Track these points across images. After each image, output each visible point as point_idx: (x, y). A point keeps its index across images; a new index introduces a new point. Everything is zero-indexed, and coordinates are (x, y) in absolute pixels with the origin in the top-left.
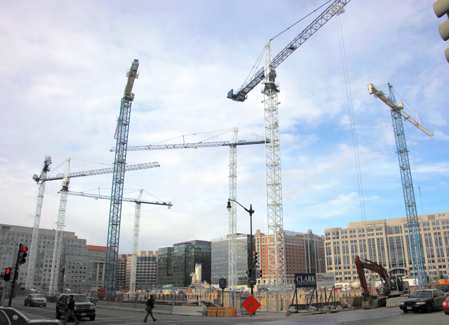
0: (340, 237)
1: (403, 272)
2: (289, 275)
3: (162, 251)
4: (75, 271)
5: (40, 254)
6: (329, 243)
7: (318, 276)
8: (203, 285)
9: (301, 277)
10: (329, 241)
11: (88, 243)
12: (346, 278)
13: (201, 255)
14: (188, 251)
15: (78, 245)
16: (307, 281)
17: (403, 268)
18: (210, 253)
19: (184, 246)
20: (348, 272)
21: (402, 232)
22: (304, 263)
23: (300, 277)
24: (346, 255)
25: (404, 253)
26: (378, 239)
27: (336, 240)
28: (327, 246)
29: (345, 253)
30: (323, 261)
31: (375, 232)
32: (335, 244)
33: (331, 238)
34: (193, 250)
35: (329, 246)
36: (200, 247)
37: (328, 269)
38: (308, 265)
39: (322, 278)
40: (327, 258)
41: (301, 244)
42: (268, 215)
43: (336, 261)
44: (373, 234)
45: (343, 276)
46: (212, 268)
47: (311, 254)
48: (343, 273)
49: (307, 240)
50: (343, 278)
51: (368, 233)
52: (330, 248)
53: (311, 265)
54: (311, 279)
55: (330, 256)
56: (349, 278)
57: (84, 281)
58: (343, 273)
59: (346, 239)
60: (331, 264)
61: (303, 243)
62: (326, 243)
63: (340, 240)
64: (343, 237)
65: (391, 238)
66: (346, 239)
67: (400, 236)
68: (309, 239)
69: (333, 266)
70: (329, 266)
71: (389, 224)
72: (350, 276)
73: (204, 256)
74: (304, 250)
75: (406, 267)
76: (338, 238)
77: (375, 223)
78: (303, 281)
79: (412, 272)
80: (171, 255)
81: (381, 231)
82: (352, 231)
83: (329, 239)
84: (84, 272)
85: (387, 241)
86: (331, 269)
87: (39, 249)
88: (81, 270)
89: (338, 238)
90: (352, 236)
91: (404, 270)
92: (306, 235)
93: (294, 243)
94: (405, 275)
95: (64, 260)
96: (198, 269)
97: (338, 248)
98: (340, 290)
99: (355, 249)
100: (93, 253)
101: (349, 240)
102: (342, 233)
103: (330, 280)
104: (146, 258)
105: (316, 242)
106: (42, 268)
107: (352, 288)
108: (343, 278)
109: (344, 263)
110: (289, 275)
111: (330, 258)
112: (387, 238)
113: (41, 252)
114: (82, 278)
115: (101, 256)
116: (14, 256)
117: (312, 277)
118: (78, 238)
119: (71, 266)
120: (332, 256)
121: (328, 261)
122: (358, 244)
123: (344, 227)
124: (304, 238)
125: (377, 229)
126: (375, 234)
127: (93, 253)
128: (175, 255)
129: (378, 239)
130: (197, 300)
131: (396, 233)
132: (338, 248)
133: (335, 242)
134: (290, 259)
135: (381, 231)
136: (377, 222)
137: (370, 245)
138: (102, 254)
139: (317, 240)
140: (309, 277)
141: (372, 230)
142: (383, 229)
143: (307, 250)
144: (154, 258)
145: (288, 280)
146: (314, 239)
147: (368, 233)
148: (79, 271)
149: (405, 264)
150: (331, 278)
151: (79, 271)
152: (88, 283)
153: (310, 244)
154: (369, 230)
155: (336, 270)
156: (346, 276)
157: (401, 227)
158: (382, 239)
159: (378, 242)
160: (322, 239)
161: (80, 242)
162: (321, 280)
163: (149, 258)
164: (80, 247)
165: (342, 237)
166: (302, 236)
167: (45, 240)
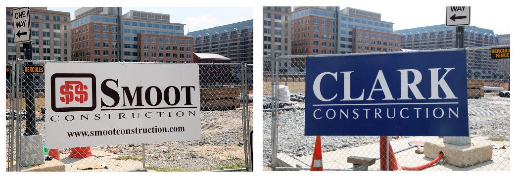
7: (60, 82)
9: (347, 75)
11: (172, 21)
16: (388, 96)
23: (341, 77)
39: (100, 94)
54: (425, 86)
78: (354, 94)
103: (163, 103)
117: (434, 72)
118: (171, 21)
130: (26, 33)
140: (404, 73)
150: (172, 93)
162: (89, 103)
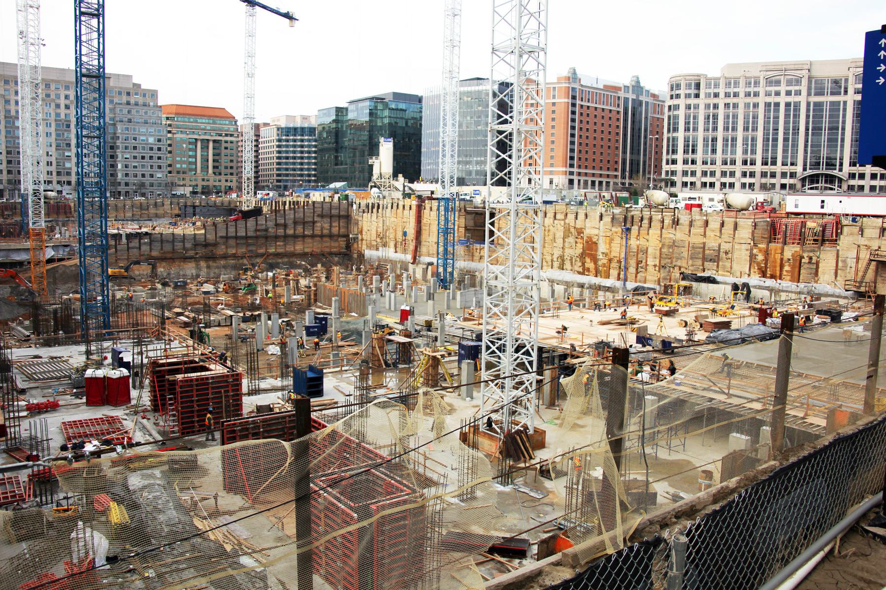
0: (702, 95)
1: (832, 182)
2: (583, 171)
3: (325, 114)
4: (139, 156)
5: (60, 120)
6: (677, 107)
8: (396, 184)
10: (675, 102)
11: (143, 87)
12: (704, 185)
13: (402, 124)
14: (376, 114)
15: (141, 102)
17: (836, 172)
18: (421, 118)
19: (367, 103)
20: (711, 172)
21: (846, 92)
22: (617, 148)
24: (710, 134)
25: (843, 140)
26: (788, 105)
27: (692, 101)
28: (671, 113)
29: (708, 130)
30: (659, 147)
31: (783, 88)
32: (690, 108)
33: (683, 96)
34: (386, 113)
35: (676, 113)
36: (402, 106)
37: (667, 163)
38: (624, 152)
40: (668, 139)
41: (614, 106)
42: (494, 11)
43: (686, 146)
44: (778, 94)
45: (698, 179)
46: (423, 150)
47: (633, 129)
48: (699, 174)
49: (628, 99)
50: (698, 184)
51: (769, 89)
52: (676, 117)
53: (632, 153)
55: (675, 135)
56: (711, 183)
57: (159, 175)
58: (699, 174)
59: (716, 101)
60: (674, 152)
61: (618, 106)
62: (670, 107)
63: (702, 101)
64: (710, 94)
65: (818, 105)
66: (716, 101)
67: (839, 102)
68: (631, 96)
69: (680, 156)
70: (669, 157)
71: (817, 73)
72: (712, 180)
73: (409, 124)
74: (618, 120)
75: (841, 170)
76: (697, 96)
77: (788, 67)
79: (852, 182)
80: (342, 122)
81: (797, 88)
82: (730, 83)
83: (678, 96)
84: (159, 158)
85: (808, 110)
86: (674, 162)
87: (58, 111)
88: (151, 153)
89: (697, 96)
90: (729, 93)
91: (835, 177)
92: (626, 87)
93: (592, 102)
94: (836, 187)
95: (115, 133)
96: (386, 148)
97: (695, 118)
98: (698, 209)
99: (733, 123)
100: (186, 120)
101: (721, 101)
102: (708, 85)
104: (295, 129)
105: (647, 103)
106: (70, 150)
107: (729, 206)
108: (698, 184)
109: (705, 152)
110: (583, 171)
111: (675, 139)
112: (808, 104)
113: (63, 117)
114: (155, 168)
115: (203, 126)
116: (6, 127)
119: (131, 146)
120: (681, 135)
121: (668, 146)
122: (741, 112)
123: (713, 70)
124: (621, 94)
125: (789, 83)
126: (783, 93)
127: (186, 120)
128: (350, 122)
129: (788, 105)
131: (832, 94)
132: (695, 118)
133: (690, 105)
134: (587, 137)
135: (797, 88)
136: (792, 67)
137: (767, 118)
138: (204, 121)
139: (650, 100)
141: (778, 83)
142: (805, 82)
143: (626, 120)
144: (312, 131)
145: (579, 181)
146: (643, 98)
147: (769, 89)
148: (147, 156)
149: (841, 164)
151: (147, 156)
152: (169, 180)
153: (634, 109)
154: (770, 82)
155: (686, 166)
156: (704, 180)
157: (846, 80)
158: (797, 105)
159: (787, 110)
160: (660, 99)
161: (144, 95)
163: (303, 129)
164: (145, 105)
165: (708, 95)
166: (619, 89)
167: (67, 92)
